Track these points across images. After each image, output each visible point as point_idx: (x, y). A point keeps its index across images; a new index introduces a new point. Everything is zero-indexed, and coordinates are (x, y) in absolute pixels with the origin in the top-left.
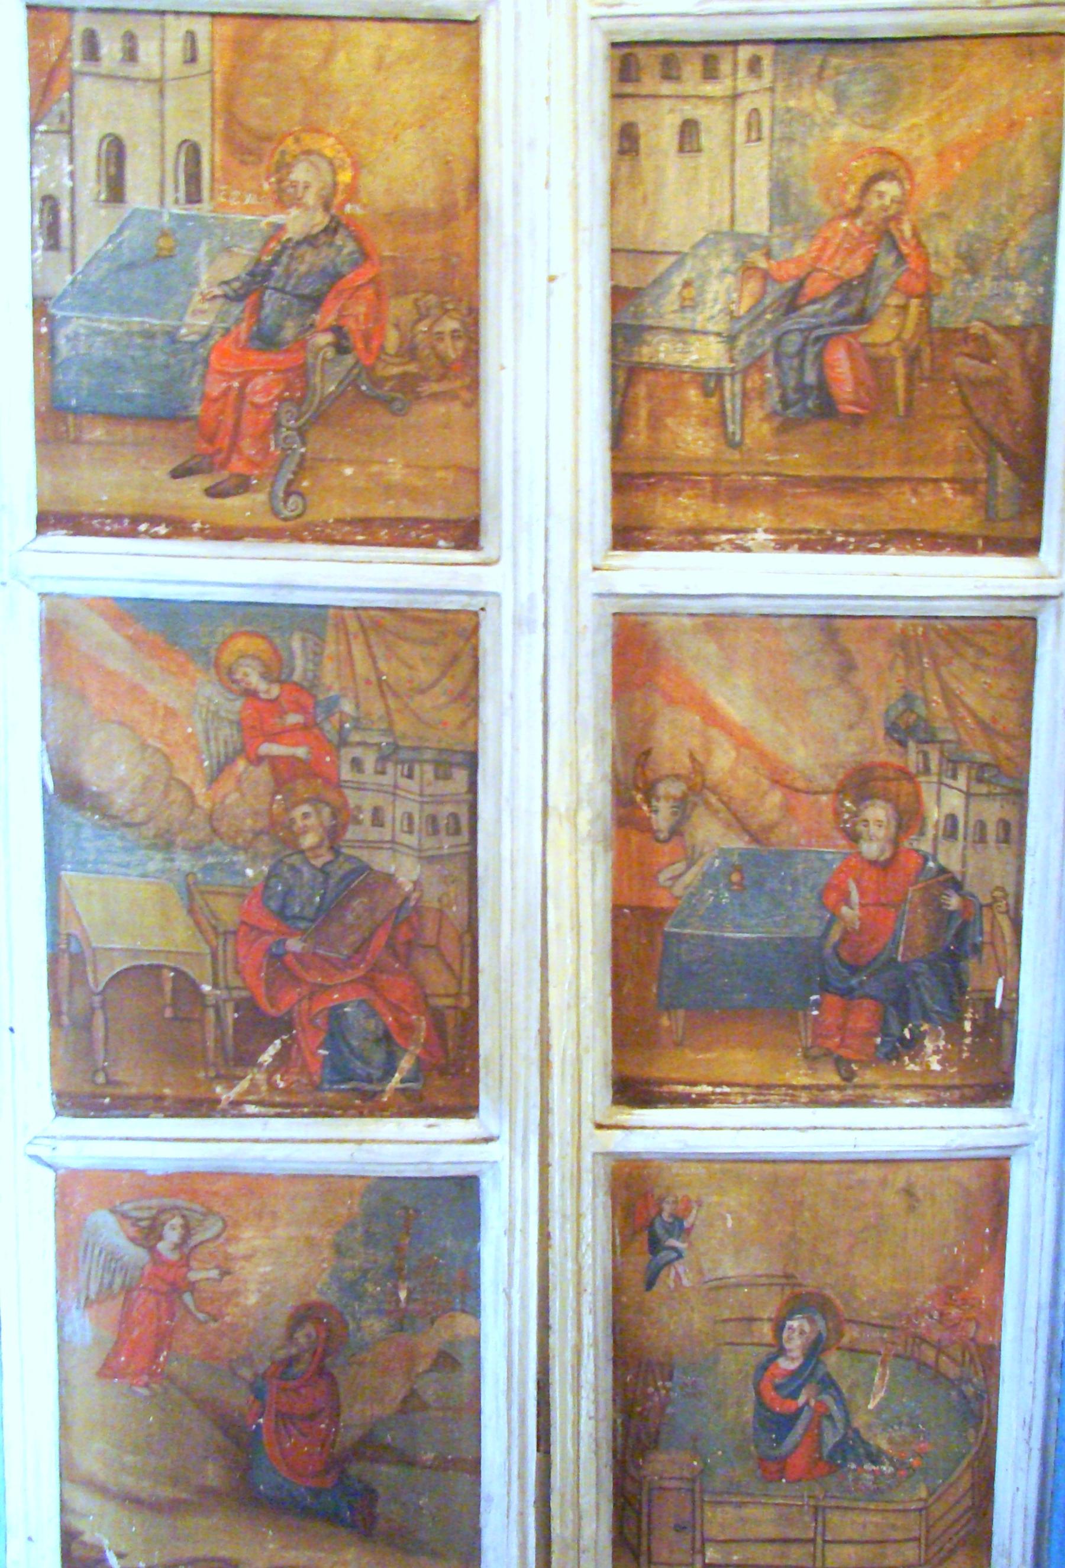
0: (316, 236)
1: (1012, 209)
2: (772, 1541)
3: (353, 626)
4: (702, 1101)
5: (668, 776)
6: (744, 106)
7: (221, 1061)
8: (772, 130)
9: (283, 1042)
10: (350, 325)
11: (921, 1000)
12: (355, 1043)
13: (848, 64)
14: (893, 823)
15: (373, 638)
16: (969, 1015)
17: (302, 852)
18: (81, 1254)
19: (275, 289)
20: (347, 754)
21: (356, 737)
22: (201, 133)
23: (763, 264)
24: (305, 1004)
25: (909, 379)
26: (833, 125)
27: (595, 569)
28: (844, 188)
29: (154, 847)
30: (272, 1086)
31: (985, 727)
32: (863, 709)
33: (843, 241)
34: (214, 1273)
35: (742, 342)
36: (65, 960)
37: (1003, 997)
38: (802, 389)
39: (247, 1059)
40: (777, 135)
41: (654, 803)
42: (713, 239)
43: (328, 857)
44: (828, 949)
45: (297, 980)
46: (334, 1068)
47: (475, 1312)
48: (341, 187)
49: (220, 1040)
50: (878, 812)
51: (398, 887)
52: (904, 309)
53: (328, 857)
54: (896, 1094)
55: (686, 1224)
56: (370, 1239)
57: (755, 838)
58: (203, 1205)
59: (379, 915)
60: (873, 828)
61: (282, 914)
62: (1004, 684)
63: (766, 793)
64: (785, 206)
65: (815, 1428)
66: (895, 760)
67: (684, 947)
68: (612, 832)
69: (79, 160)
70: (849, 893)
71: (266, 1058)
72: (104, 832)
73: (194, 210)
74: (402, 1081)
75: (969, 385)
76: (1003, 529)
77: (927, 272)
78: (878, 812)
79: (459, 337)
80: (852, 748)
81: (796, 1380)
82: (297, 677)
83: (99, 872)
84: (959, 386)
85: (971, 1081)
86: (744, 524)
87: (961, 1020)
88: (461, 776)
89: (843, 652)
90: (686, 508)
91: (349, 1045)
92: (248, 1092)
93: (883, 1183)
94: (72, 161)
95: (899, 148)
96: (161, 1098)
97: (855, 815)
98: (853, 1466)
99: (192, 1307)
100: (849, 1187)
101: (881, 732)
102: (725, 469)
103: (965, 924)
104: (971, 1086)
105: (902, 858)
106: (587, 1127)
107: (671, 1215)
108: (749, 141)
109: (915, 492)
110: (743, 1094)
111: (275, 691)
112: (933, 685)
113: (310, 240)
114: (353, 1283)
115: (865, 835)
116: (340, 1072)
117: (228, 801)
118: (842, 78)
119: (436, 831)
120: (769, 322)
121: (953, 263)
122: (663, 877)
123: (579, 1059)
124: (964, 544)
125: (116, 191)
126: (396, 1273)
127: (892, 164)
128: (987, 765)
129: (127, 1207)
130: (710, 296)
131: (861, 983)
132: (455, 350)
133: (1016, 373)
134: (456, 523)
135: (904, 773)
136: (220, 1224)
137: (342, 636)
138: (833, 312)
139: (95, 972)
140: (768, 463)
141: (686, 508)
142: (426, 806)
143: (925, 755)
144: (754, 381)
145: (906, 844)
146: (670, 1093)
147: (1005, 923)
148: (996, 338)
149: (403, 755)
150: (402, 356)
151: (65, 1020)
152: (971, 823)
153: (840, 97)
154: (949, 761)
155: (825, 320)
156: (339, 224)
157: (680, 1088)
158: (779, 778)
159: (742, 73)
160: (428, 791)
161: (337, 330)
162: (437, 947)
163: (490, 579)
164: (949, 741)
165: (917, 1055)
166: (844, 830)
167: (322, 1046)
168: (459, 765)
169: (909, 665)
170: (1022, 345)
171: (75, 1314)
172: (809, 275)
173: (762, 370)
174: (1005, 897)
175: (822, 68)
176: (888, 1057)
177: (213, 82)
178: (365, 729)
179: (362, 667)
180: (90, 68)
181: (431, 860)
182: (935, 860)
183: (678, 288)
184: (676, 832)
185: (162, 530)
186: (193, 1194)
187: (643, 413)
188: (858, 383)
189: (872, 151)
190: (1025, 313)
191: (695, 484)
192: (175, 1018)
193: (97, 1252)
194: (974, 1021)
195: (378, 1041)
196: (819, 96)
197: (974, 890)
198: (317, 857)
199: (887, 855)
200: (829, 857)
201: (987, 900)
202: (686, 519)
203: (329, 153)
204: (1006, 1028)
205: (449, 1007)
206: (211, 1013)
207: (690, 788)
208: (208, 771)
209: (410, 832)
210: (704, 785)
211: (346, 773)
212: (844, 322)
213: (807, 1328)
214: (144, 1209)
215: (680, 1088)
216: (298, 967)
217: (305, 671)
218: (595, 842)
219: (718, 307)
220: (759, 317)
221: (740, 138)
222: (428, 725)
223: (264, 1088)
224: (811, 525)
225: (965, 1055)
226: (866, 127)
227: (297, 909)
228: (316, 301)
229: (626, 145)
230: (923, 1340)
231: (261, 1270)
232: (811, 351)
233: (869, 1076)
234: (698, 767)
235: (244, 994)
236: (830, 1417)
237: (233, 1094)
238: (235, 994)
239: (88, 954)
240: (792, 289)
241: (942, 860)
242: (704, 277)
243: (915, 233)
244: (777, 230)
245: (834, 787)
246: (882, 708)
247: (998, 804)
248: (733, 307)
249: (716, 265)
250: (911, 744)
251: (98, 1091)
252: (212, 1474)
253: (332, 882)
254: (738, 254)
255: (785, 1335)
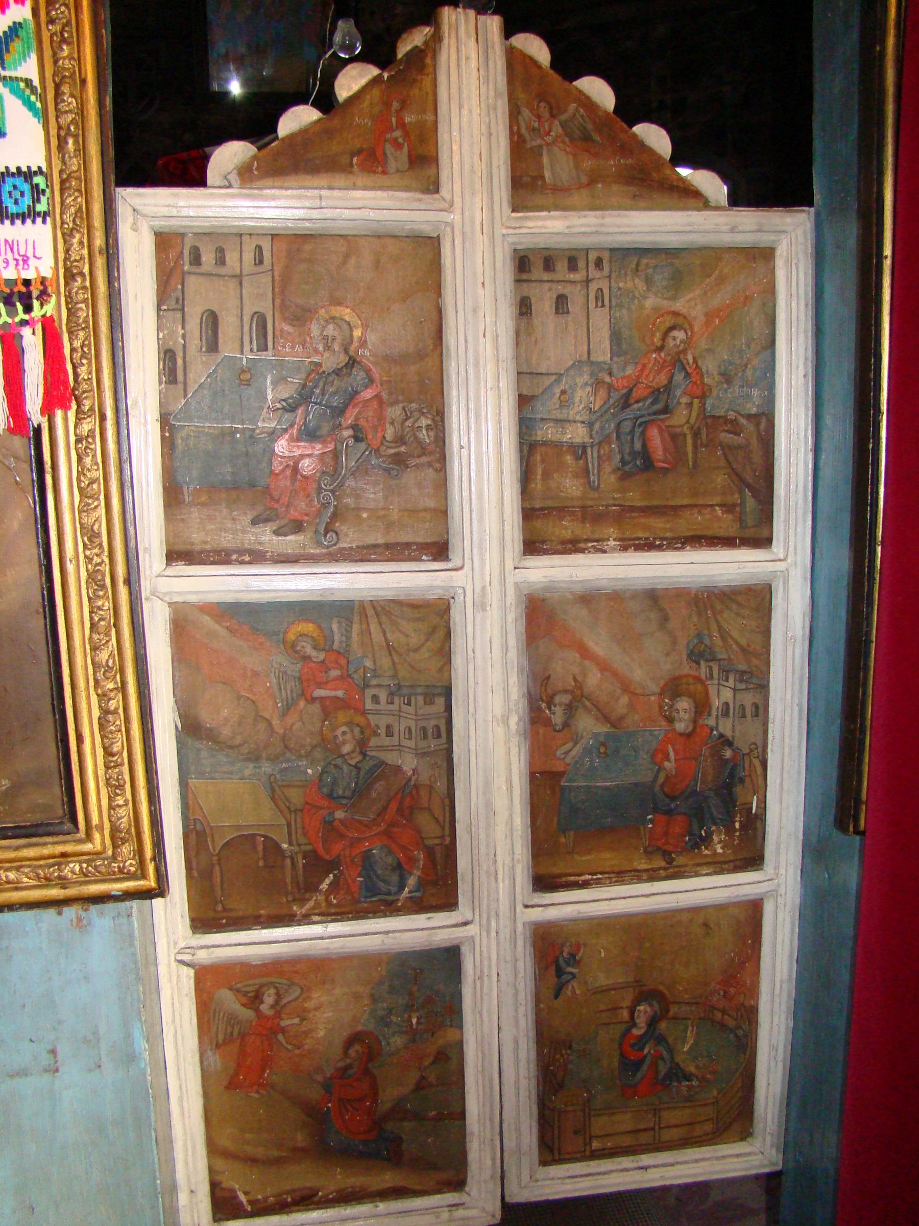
0: (340, 369)
1: (749, 346)
2: (629, 1132)
3: (370, 612)
4: (585, 885)
5: (561, 691)
6: (593, 287)
7: (296, 891)
8: (610, 301)
9: (335, 875)
10: (362, 423)
11: (711, 814)
12: (379, 872)
13: (653, 262)
14: (693, 710)
15: (384, 619)
16: (738, 819)
17: (343, 756)
18: (212, 1015)
19: (316, 403)
20: (369, 692)
21: (374, 682)
22: (265, 307)
23: (607, 379)
24: (347, 852)
25: (695, 447)
26: (645, 298)
27: (515, 568)
28: (653, 335)
29: (248, 760)
30: (329, 903)
31: (743, 650)
32: (674, 643)
33: (654, 364)
34: (297, 1021)
35: (597, 426)
36: (193, 836)
37: (757, 807)
38: (634, 454)
39: (311, 887)
40: (613, 303)
41: (553, 708)
42: (578, 365)
43: (359, 758)
44: (657, 789)
45: (342, 836)
46: (368, 890)
47: (460, 1027)
48: (355, 339)
49: (295, 878)
50: (684, 705)
51: (404, 773)
52: (690, 405)
53: (359, 758)
54: (698, 868)
55: (577, 958)
56: (392, 990)
57: (613, 726)
58: (288, 979)
59: (392, 793)
60: (682, 714)
61: (330, 796)
62: (753, 624)
63: (619, 698)
64: (619, 345)
65: (654, 1064)
66: (695, 673)
67: (573, 794)
68: (528, 727)
69: (188, 327)
70: (669, 754)
71: (324, 886)
72: (215, 753)
73: (263, 355)
74: (410, 892)
75: (728, 449)
76: (750, 533)
77: (703, 383)
78: (684, 705)
79: (432, 429)
80: (668, 667)
81: (642, 1041)
82: (336, 646)
83: (213, 778)
84: (723, 449)
85: (740, 857)
86: (601, 536)
87: (734, 822)
88: (440, 701)
89: (661, 610)
90: (567, 528)
91: (375, 872)
92: (313, 908)
93: (691, 921)
94: (183, 328)
95: (684, 311)
96: (260, 916)
97: (671, 707)
98: (676, 1084)
99: (284, 1042)
100: (672, 926)
101: (685, 657)
102: (589, 503)
103: (735, 765)
104: (740, 860)
105: (698, 730)
106: (519, 907)
107: (569, 953)
108: (597, 306)
109: (700, 512)
110: (609, 878)
111: (322, 656)
112: (714, 627)
113: (337, 372)
114: (382, 1018)
115: (677, 718)
116: (372, 890)
117: (294, 727)
118: (650, 271)
119: (425, 737)
120: (613, 414)
121: (717, 378)
122: (558, 753)
123: (513, 868)
124: (728, 542)
125: (213, 346)
126: (410, 1008)
127: (680, 320)
128: (745, 672)
129: (239, 985)
130: (577, 400)
131: (677, 805)
132: (429, 436)
133: (754, 442)
134: (434, 544)
135: (698, 679)
136: (299, 990)
137: (363, 619)
138: (649, 407)
139: (213, 841)
140: (614, 499)
141: (567, 528)
142: (419, 722)
143: (711, 668)
144: (605, 449)
145: (701, 722)
146: (566, 882)
147: (757, 763)
148: (743, 421)
149: (405, 691)
150: (396, 442)
151: (195, 873)
152: (737, 706)
153: (649, 281)
154: (724, 671)
155: (645, 412)
156: (354, 361)
157: (572, 878)
158: (626, 687)
159: (592, 267)
160: (420, 712)
161: (355, 427)
162: (429, 809)
163: (459, 579)
164: (724, 659)
165: (709, 845)
166: (664, 716)
167: (360, 875)
168: (439, 695)
169: (699, 614)
170: (758, 425)
171: (210, 1053)
172: (635, 385)
173: (610, 444)
174: (757, 749)
175: (638, 265)
176: (693, 848)
177: (273, 277)
178: (379, 677)
179: (377, 636)
180: (194, 269)
181: (424, 754)
182: (717, 729)
183: (558, 395)
184: (566, 725)
185: (247, 558)
186: (281, 974)
187: (539, 471)
188: (665, 450)
189: (669, 313)
190: (758, 406)
191: (573, 513)
192: (265, 866)
193: (221, 1015)
194: (740, 822)
195: (393, 869)
196: (637, 281)
197: (739, 746)
198: (352, 758)
199: (690, 728)
200: (656, 733)
201: (746, 751)
202: (567, 534)
203: (347, 318)
204: (759, 824)
205: (437, 845)
206: (288, 861)
207: (574, 698)
208: (281, 709)
209: (410, 739)
210: (582, 696)
211: (369, 705)
212: (655, 413)
213: (649, 1009)
214: (250, 986)
215: (572, 878)
216: (342, 828)
217: (341, 642)
218: (520, 735)
219: (582, 406)
220: (606, 412)
221: (592, 305)
222: (420, 671)
223: (324, 905)
224: (640, 535)
225: (736, 842)
226: (665, 299)
227: (340, 792)
228: (340, 411)
229: (524, 310)
230: (714, 1008)
231: (326, 1015)
232: (638, 431)
233: (680, 860)
234: (579, 685)
235: (310, 847)
236: (662, 1059)
237: (304, 911)
238: (303, 848)
239: (208, 831)
240: (624, 395)
241: (721, 729)
242: (573, 388)
243: (694, 358)
244: (615, 359)
245: (658, 690)
246: (685, 642)
247: (751, 694)
248: (592, 406)
249: (580, 381)
250: (702, 662)
251: (219, 915)
252: (301, 1139)
253: (362, 773)
254: (592, 374)
255: (636, 1014)
